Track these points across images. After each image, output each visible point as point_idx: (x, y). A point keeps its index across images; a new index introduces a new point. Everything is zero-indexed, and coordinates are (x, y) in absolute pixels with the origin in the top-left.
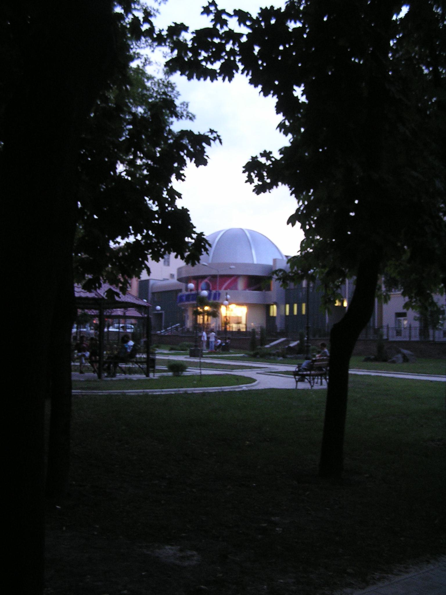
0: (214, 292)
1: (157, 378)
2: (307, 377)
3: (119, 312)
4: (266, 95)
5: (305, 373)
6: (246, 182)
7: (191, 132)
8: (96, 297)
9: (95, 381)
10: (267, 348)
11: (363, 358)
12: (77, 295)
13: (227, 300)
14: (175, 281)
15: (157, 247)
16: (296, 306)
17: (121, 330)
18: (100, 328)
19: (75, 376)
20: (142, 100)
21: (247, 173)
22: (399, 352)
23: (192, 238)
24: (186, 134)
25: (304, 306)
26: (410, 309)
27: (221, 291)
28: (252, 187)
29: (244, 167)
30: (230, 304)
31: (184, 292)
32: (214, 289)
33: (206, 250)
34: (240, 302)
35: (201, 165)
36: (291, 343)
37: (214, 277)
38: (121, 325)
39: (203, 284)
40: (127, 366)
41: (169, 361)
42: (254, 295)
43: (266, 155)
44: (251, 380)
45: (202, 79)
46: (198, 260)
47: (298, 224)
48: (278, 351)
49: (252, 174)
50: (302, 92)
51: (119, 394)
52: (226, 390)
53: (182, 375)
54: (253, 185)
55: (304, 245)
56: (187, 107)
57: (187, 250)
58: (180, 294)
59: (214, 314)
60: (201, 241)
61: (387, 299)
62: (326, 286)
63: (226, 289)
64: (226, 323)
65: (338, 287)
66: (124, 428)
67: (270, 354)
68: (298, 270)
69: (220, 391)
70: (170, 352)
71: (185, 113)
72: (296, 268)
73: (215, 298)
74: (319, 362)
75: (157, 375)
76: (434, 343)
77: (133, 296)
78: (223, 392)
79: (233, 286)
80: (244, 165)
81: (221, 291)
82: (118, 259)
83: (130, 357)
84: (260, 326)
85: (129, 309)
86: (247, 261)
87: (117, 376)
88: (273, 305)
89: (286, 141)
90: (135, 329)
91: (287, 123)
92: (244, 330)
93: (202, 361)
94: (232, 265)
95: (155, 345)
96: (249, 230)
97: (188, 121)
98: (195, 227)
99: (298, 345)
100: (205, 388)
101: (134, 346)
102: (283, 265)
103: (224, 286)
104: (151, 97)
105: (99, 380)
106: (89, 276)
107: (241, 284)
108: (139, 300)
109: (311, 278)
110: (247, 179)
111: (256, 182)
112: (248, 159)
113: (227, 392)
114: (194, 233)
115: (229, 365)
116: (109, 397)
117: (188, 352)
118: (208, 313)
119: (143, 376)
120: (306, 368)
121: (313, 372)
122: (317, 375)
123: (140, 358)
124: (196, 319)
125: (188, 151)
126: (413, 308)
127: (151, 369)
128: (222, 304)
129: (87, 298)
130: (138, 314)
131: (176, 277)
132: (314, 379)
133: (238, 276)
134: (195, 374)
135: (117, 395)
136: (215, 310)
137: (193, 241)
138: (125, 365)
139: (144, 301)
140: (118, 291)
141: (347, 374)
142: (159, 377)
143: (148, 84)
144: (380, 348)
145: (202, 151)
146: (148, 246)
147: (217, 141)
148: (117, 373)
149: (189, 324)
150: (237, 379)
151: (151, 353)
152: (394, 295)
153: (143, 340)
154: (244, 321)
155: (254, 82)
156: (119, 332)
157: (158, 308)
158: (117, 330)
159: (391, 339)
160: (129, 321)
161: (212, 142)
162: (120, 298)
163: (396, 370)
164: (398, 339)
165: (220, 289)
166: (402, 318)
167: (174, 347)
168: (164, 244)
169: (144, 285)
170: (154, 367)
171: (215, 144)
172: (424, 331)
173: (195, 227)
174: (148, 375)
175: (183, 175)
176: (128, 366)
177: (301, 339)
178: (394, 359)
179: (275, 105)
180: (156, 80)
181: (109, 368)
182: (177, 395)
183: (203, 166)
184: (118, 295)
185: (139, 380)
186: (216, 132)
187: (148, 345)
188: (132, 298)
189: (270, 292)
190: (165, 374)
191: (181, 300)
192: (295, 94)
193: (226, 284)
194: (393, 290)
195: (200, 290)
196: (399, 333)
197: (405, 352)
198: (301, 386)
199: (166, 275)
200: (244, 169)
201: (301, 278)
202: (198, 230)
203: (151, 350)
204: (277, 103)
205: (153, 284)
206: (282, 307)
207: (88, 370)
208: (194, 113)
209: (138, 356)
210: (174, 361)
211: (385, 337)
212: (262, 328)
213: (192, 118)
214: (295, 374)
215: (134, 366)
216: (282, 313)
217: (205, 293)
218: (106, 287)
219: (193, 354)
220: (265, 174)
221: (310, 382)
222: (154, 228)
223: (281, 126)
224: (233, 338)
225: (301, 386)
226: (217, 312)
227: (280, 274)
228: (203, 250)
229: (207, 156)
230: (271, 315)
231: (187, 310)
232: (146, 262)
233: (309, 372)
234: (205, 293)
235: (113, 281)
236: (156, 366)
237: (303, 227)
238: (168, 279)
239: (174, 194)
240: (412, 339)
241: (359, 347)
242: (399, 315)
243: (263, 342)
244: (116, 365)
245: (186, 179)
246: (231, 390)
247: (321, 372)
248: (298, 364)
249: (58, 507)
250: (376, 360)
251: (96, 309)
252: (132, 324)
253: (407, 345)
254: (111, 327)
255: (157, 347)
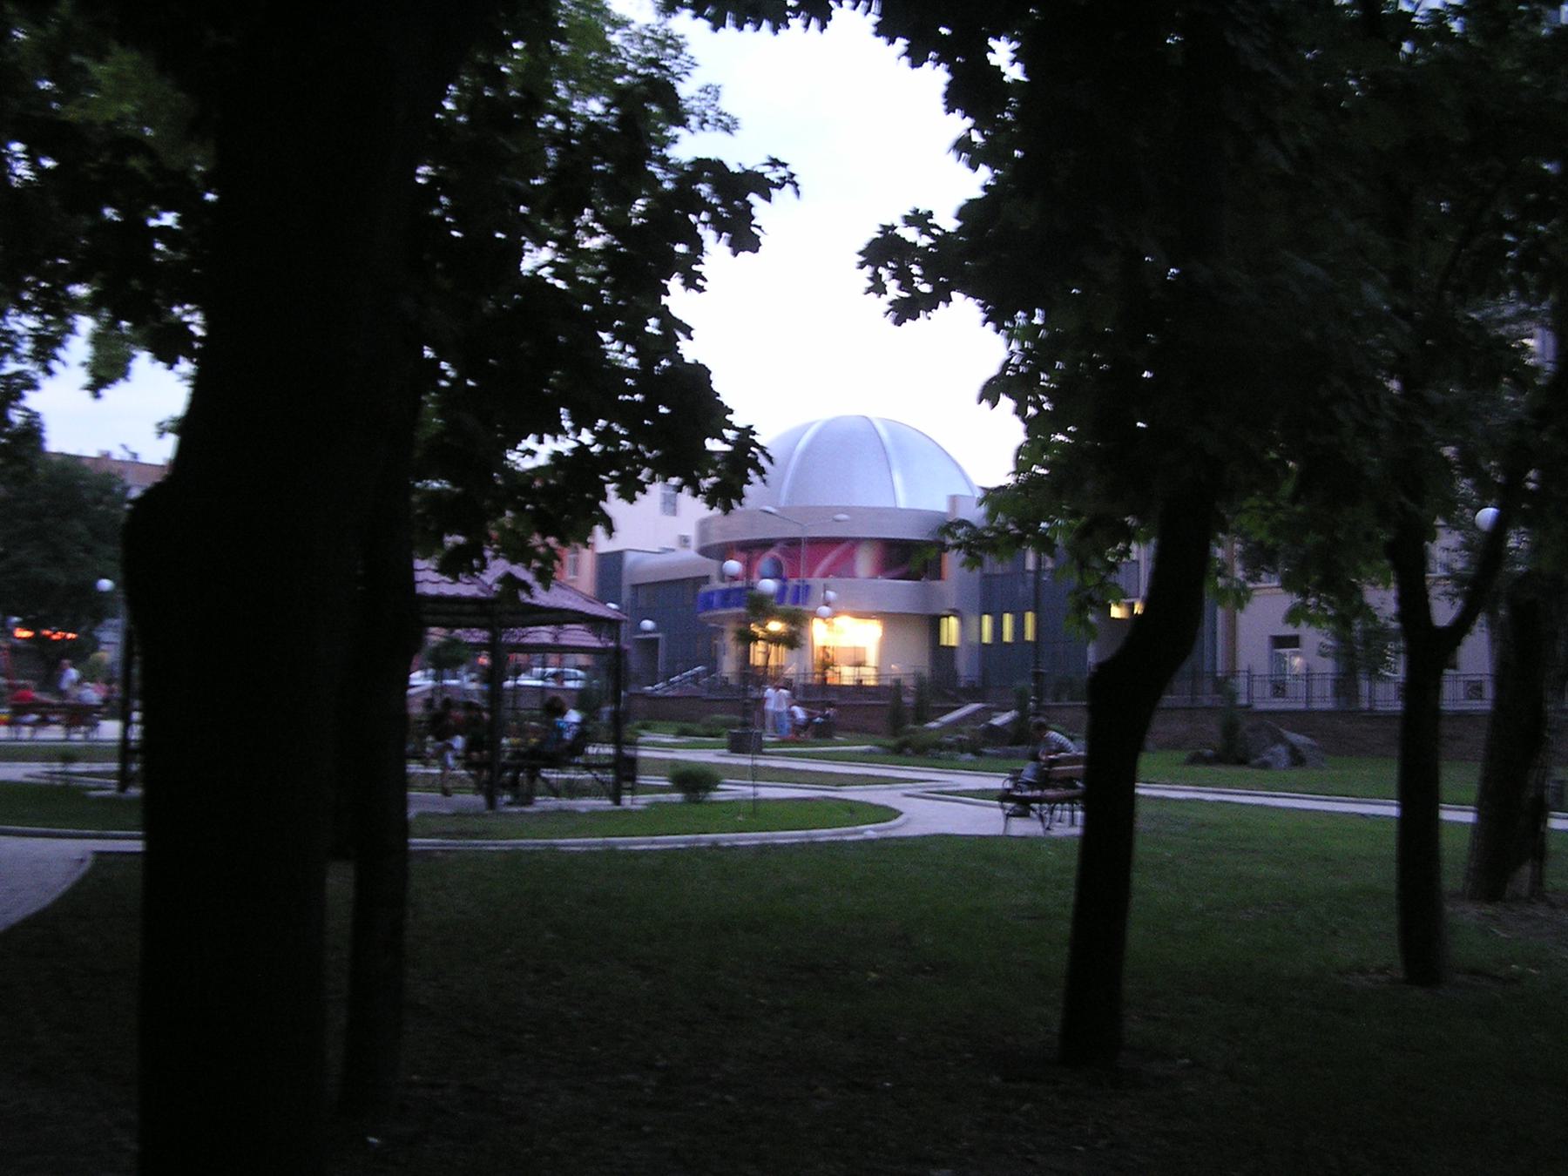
0: (793, 582)
1: (640, 807)
2: (1033, 805)
3: (544, 635)
4: (916, 63)
5: (1029, 793)
6: (869, 290)
7: (720, 165)
8: (482, 595)
9: (477, 815)
10: (931, 729)
11: (1183, 756)
12: (429, 589)
13: (827, 604)
14: (691, 553)
15: (633, 464)
16: (1008, 620)
17: (551, 684)
18: (493, 677)
19: (420, 802)
20: (596, 79)
21: (868, 270)
22: (1281, 739)
23: (726, 441)
24: (710, 168)
25: (1030, 618)
26: (1303, 624)
27: (812, 581)
28: (883, 303)
29: (861, 253)
30: (835, 614)
31: (717, 585)
32: (795, 575)
33: (761, 471)
34: (866, 608)
35: (743, 251)
36: (995, 717)
37: (793, 543)
38: (550, 670)
39: (764, 563)
40: (560, 776)
41: (674, 763)
42: (899, 592)
43: (919, 220)
44: (890, 813)
45: (748, 27)
46: (740, 496)
47: (1006, 403)
48: (961, 736)
49: (881, 270)
50: (1013, 56)
51: (538, 848)
52: (822, 839)
53: (707, 799)
54: (886, 299)
55: (1024, 458)
56: (717, 99)
57: (710, 472)
58: (705, 589)
59: (791, 641)
60: (745, 448)
61: (1240, 597)
62: (1083, 566)
63: (825, 575)
64: (827, 664)
65: (1113, 567)
66: (549, 935)
67: (939, 746)
68: (1007, 523)
69: (805, 840)
70: (676, 740)
71: (710, 113)
72: (1001, 517)
73: (796, 600)
74: (1066, 765)
75: (642, 800)
76: (1373, 716)
77: (582, 594)
78: (813, 843)
79: (842, 568)
80: (862, 247)
81: (812, 581)
82: (532, 495)
83: (567, 752)
84: (912, 670)
85: (568, 626)
86: (883, 502)
87: (535, 803)
88: (948, 617)
89: (974, 182)
90: (588, 680)
91: (976, 137)
92: (872, 683)
93: (761, 763)
94: (839, 513)
95: (638, 723)
96: (885, 421)
97: (721, 135)
98: (731, 412)
99: (1013, 722)
100: (767, 834)
101: (582, 723)
102: (975, 514)
103: (821, 568)
104: (623, 71)
105: (487, 812)
106: (453, 540)
107: (864, 562)
108: (593, 603)
109: (1045, 545)
110: (870, 284)
111: (893, 290)
112: (873, 232)
113: (823, 842)
114: (730, 426)
115: (831, 774)
116: (514, 857)
117: (724, 740)
118: (774, 639)
119: (605, 804)
120: (1033, 781)
121: (1050, 793)
122: (1062, 800)
123: (597, 755)
124: (746, 655)
125: (711, 209)
126: (1311, 620)
127: (628, 785)
128: (815, 615)
129: (457, 600)
130: (591, 641)
131: (694, 544)
132: (1052, 811)
133: (857, 542)
134: (740, 797)
135: (533, 852)
136: (794, 629)
137: (727, 448)
138: (575, 774)
139: (611, 608)
140: (528, 577)
141: (1132, 798)
142: (646, 804)
143: (616, 39)
144: (1230, 730)
145: (746, 214)
146: (609, 460)
147: (788, 188)
148: (537, 795)
149: (728, 666)
150: (852, 811)
151: (627, 744)
152: (1267, 590)
153: (607, 709)
154: (872, 658)
155: (886, 30)
156: (542, 689)
157: (648, 624)
158: (540, 683)
159: (1260, 706)
160: (571, 658)
161: (774, 191)
162: (532, 597)
163: (1271, 787)
164: (1279, 704)
165: (810, 575)
166: (1287, 651)
167: (687, 725)
168: (648, 455)
169: (611, 565)
170: (633, 779)
171: (782, 196)
172: (1345, 684)
173: (731, 412)
174: (617, 802)
175: (699, 275)
176: (565, 776)
177: (1022, 708)
178: (1268, 758)
179: (943, 89)
180: (634, 27)
181: (514, 782)
182: (695, 852)
183: (747, 253)
184: (527, 587)
185: (594, 814)
186: (784, 165)
187: (618, 720)
188: (575, 597)
189: (937, 583)
190: (662, 797)
191: (708, 603)
192: (993, 59)
193: (826, 562)
194: (1264, 576)
195: (755, 579)
196: (1279, 689)
197: (1294, 737)
198: (1020, 827)
199: (670, 541)
200: (861, 259)
201: (1019, 541)
202: (738, 419)
203: (628, 736)
204: (950, 84)
205: (1387, 588)
206: (974, 621)
207: (461, 788)
208: (735, 114)
209: (591, 750)
210: (686, 762)
211: (1243, 701)
212: (920, 681)
213: (728, 126)
214: (1004, 796)
215: (580, 777)
216: (974, 639)
217: (769, 585)
218: (498, 568)
219: (737, 746)
220: (916, 270)
221: (1041, 818)
222: (629, 414)
223: (963, 145)
224: (844, 703)
225: (1020, 827)
226: (799, 634)
227: (960, 532)
228: (750, 471)
229: (760, 227)
230: (944, 642)
231: (722, 631)
232: (602, 503)
233: (1038, 793)
234: (769, 585)
235: (519, 553)
236: (641, 777)
237: (1020, 411)
238: (673, 550)
239: (674, 327)
240: (1316, 706)
241: (1160, 727)
242: (1280, 642)
243: (922, 713)
244: (534, 775)
245: (706, 285)
246: (834, 838)
247: (1070, 792)
248: (1011, 771)
249: (372, 1140)
250: (1218, 759)
251: (481, 627)
252: (579, 668)
253: (1302, 720)
254: (523, 676)
255: (645, 727)
